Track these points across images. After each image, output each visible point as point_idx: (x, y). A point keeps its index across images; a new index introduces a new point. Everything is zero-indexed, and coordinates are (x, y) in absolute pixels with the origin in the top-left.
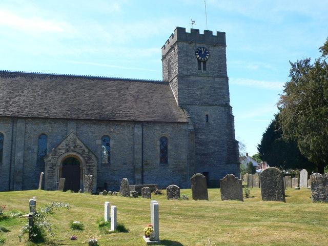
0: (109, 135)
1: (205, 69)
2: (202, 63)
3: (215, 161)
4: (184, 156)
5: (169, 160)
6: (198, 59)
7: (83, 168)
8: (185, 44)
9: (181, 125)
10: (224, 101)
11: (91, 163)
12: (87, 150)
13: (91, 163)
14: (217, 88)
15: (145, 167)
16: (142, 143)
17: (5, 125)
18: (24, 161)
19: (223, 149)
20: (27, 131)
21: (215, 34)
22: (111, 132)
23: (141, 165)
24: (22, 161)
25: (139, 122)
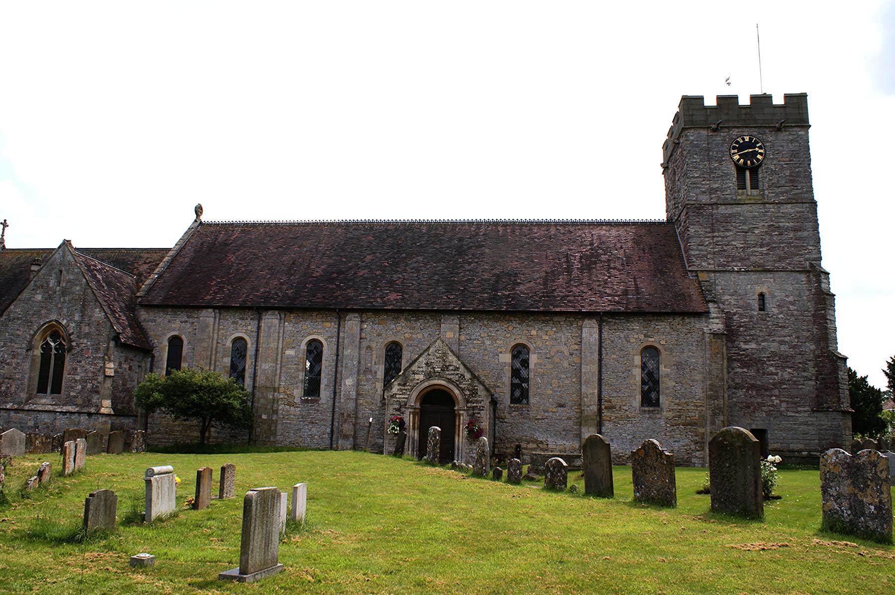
0: (526, 343)
1: (755, 186)
2: (748, 173)
3: (784, 405)
4: (698, 391)
5: (662, 399)
6: (735, 164)
7: (461, 412)
8: (704, 132)
9: (692, 320)
10: (807, 260)
11: (477, 402)
12: (468, 376)
13: (477, 402)
14: (787, 229)
15: (606, 413)
16: (600, 360)
17: (325, 324)
18: (358, 394)
19: (805, 374)
20: (363, 335)
21: (778, 100)
22: (529, 338)
23: (595, 408)
24: (353, 394)
25: (590, 315)
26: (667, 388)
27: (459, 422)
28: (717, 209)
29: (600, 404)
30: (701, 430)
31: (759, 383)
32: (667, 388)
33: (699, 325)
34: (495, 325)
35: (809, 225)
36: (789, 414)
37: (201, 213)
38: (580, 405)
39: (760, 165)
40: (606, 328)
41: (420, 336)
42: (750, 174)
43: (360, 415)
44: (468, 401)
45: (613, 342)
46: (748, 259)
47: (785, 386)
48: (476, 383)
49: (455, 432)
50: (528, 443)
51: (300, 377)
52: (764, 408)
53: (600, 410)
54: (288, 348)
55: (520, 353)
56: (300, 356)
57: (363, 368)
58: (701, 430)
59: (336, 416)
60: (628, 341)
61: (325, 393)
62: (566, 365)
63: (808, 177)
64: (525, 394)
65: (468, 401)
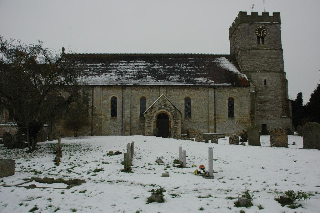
1: (263, 43)
5: (235, 115)
8: (247, 24)
9: (245, 88)
11: (177, 117)
12: (173, 108)
13: (177, 117)
15: (217, 120)
16: (215, 102)
19: (279, 106)
20: (132, 95)
22: (191, 95)
23: (213, 118)
24: (129, 116)
26: (237, 111)
27: (171, 124)
28: (251, 51)
29: (215, 117)
30: (248, 125)
31: (264, 109)
32: (237, 111)
33: (246, 90)
34: (179, 90)
35: (280, 57)
36: (274, 119)
37: (64, 50)
38: (208, 117)
39: (265, 36)
40: (216, 91)
41: (152, 95)
42: (262, 39)
43: (132, 123)
44: (174, 117)
45: (219, 96)
46: (261, 68)
47: (272, 110)
48: (176, 111)
49: (169, 128)
50: (191, 130)
51: (109, 110)
52: (266, 117)
53: (215, 119)
54: (104, 100)
55: (188, 100)
56: (109, 102)
57: (132, 106)
58: (248, 125)
59: (123, 123)
60: (224, 96)
61: (119, 116)
62: (203, 104)
63: (280, 40)
64: (190, 114)
65: (174, 117)
